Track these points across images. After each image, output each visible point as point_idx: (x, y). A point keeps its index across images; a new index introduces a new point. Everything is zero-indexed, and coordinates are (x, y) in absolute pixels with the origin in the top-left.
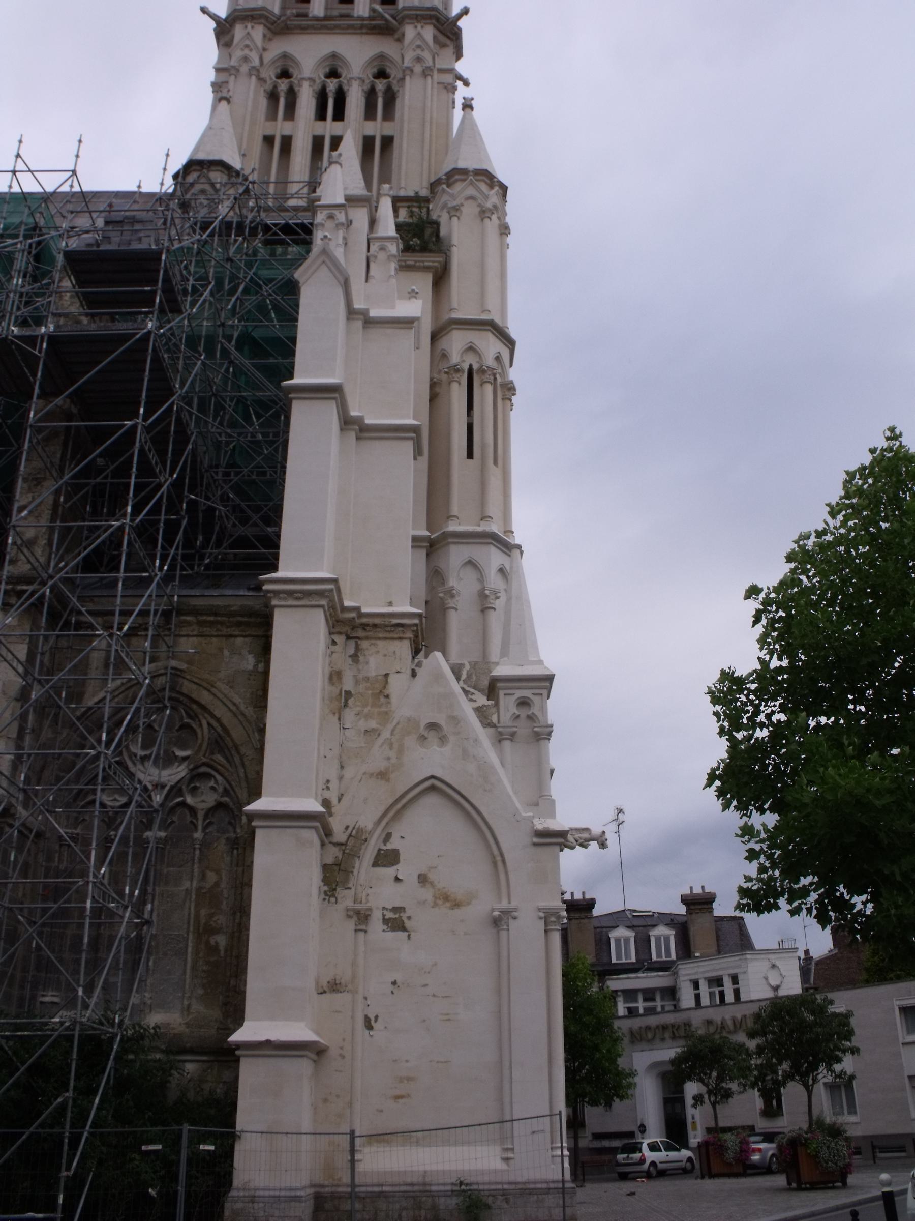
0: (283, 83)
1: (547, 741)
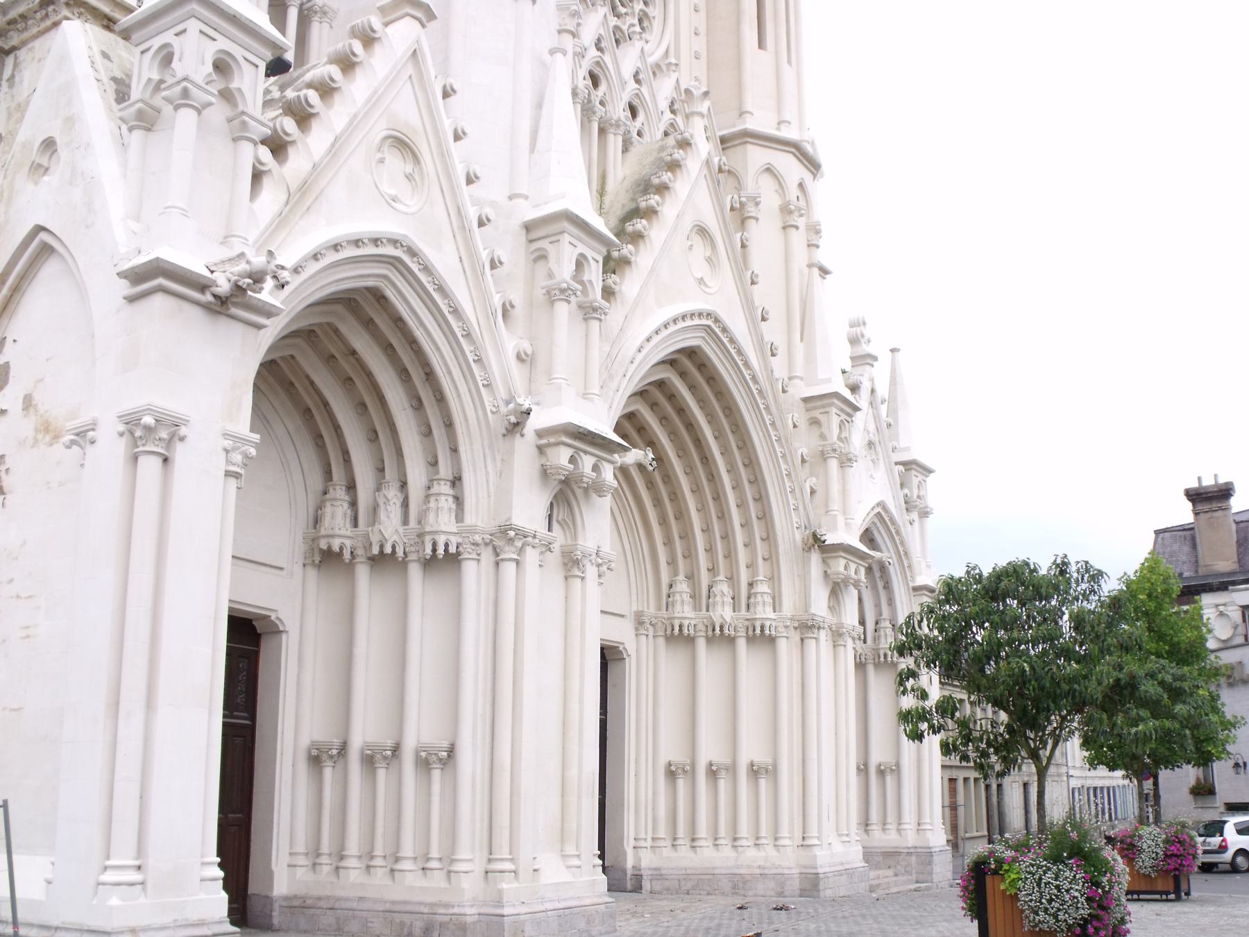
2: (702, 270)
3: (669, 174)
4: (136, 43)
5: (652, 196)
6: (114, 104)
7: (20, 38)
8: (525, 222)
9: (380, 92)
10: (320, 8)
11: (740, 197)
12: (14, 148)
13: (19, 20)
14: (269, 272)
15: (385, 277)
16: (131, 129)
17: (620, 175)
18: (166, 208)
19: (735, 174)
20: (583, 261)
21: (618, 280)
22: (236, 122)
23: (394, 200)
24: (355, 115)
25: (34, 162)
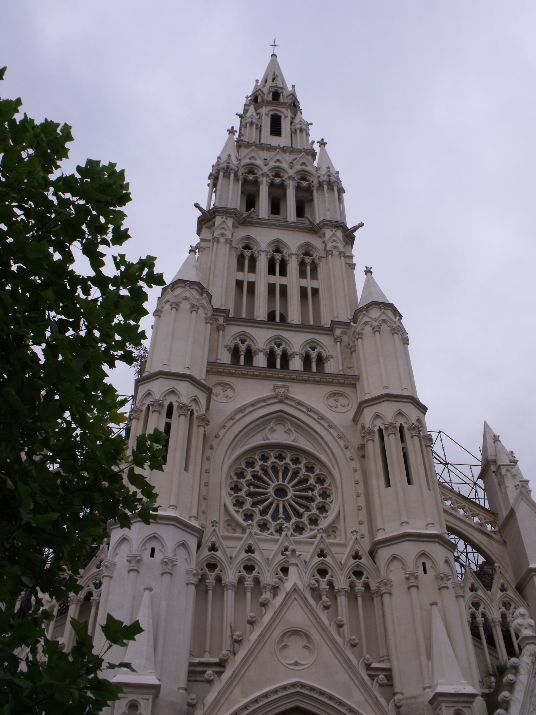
0: (247, 252)
1: (207, 685)
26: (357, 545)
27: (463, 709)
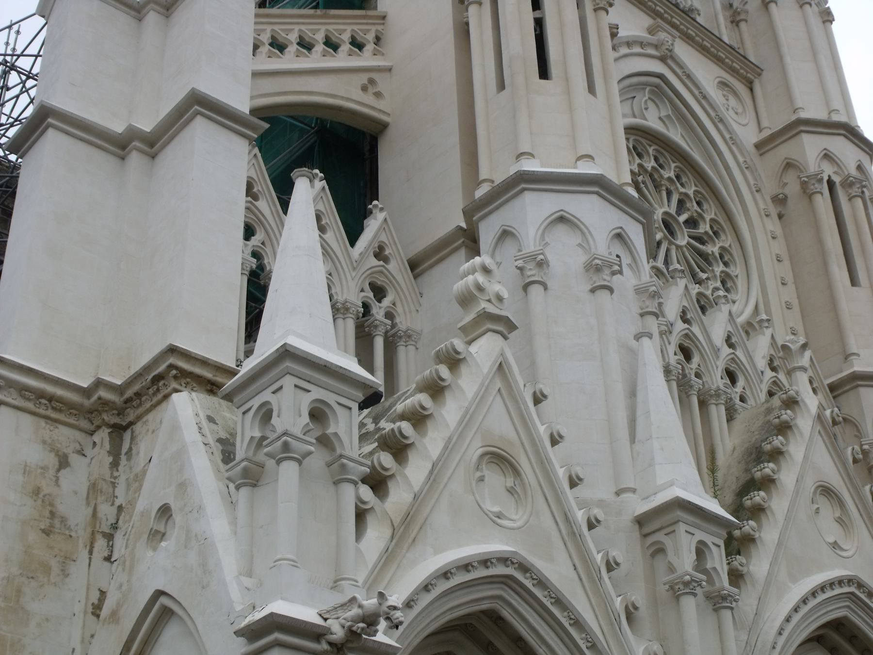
2: (834, 532)
3: (780, 437)
4: (238, 406)
5: (766, 464)
6: (221, 464)
7: (136, 414)
8: (635, 517)
9: (471, 412)
10: (405, 332)
11: (861, 445)
12: (133, 518)
13: (135, 398)
14: (382, 613)
15: (500, 597)
16: (238, 488)
17: (729, 445)
18: (276, 561)
19: (851, 421)
20: (704, 549)
21: (744, 561)
22: (336, 465)
23: (499, 517)
24: (450, 439)
25: (152, 529)
26: (384, 233)
27: (339, 410)
